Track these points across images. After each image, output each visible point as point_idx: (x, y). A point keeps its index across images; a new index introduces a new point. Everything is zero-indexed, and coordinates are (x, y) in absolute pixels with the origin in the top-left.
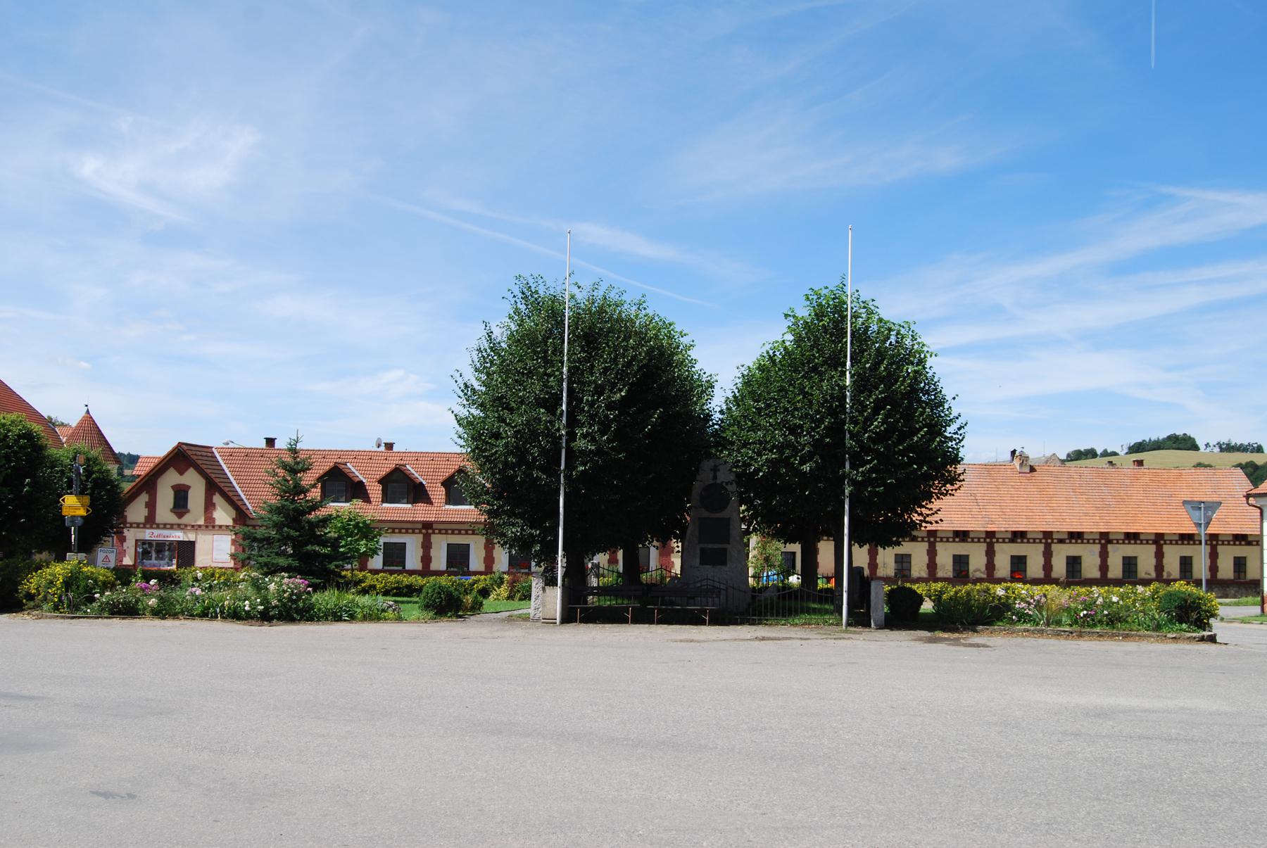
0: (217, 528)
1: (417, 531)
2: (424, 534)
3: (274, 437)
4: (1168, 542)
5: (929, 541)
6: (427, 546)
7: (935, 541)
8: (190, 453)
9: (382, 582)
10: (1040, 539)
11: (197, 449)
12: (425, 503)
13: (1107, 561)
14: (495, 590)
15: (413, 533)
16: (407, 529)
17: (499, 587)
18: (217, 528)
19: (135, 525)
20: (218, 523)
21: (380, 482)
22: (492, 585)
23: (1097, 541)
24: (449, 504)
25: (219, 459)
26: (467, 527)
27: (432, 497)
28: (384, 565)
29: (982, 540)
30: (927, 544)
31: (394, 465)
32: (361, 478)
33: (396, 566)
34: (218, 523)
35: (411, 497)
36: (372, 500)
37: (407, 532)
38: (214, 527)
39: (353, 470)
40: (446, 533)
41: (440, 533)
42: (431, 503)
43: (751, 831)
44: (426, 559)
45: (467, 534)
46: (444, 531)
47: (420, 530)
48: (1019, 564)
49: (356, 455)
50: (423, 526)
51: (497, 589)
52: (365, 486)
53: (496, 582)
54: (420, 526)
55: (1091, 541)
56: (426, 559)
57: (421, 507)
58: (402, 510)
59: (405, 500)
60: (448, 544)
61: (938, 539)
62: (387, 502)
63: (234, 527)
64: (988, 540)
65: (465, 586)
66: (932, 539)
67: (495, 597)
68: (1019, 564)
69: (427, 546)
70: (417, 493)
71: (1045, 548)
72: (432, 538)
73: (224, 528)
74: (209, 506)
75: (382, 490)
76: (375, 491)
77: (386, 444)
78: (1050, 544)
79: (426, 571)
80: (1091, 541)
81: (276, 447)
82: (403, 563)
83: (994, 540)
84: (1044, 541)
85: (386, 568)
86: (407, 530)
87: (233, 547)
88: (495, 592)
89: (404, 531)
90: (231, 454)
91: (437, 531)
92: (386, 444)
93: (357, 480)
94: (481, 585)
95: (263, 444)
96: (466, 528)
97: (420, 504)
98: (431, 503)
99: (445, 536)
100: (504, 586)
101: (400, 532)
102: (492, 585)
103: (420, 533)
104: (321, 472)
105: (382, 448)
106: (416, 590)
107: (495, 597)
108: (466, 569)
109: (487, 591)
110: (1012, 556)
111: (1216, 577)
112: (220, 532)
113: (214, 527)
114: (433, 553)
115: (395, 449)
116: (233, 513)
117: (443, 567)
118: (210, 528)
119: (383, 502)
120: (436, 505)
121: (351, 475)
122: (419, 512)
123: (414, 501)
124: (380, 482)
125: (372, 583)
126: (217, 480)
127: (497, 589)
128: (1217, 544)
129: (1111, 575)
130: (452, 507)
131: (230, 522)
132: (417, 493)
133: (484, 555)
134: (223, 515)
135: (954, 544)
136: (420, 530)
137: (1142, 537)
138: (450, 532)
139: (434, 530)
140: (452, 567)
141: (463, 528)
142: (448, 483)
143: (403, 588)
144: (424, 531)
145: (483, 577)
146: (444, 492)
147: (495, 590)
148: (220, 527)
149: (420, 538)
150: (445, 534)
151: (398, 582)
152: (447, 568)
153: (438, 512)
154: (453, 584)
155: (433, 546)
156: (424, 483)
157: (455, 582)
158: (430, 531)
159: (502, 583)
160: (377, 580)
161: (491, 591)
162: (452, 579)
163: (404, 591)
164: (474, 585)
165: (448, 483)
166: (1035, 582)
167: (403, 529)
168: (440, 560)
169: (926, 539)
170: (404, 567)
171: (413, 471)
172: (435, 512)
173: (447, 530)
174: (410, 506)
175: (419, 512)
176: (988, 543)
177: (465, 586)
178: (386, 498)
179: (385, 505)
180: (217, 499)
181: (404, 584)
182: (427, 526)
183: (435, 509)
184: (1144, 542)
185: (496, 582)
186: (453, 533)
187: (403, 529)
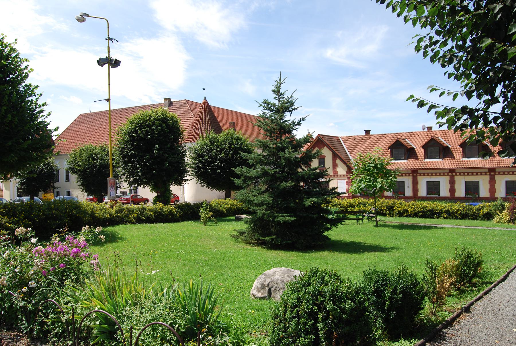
0: (339, 176)
1: (446, 174)
2: (450, 176)
3: (369, 129)
4: (458, 174)
5: (490, 175)
6: (452, 183)
7: (417, 176)
8: (324, 139)
9: (412, 207)
11: (329, 137)
12: (450, 158)
14: (498, 215)
15: (444, 175)
16: (440, 173)
17: (501, 212)
18: (339, 176)
19: (507, 173)
20: (339, 174)
21: (423, 147)
22: (495, 210)
23: (345, 176)
24: (465, 158)
25: (342, 142)
27: (454, 154)
30: (489, 176)
31: (431, 137)
32: (447, 145)
34: (339, 174)
35: (406, 156)
36: (419, 158)
37: (440, 175)
38: (337, 176)
39: (409, 142)
40: (464, 175)
41: (460, 175)
42: (454, 158)
44: (452, 190)
46: (463, 174)
47: (448, 173)
49: (410, 135)
51: (499, 214)
52: (415, 150)
53: (498, 208)
54: (447, 171)
57: (448, 160)
58: (437, 162)
59: (439, 157)
60: (465, 181)
62: (427, 158)
63: (347, 175)
65: (473, 211)
67: (498, 220)
69: (452, 183)
70: (410, 153)
71: (490, 178)
73: (342, 176)
74: (335, 166)
75: (463, 152)
76: (420, 152)
77: (427, 127)
79: (492, 198)
80: (483, 173)
81: (371, 134)
82: (438, 193)
87: (347, 186)
88: (497, 216)
89: (438, 174)
90: (347, 139)
91: (458, 174)
92: (428, 128)
93: (409, 147)
94: (486, 210)
95: (364, 133)
96: (439, 172)
97: (447, 159)
98: (454, 158)
100: (505, 212)
101: (436, 175)
102: (495, 210)
103: (448, 175)
104: (423, 143)
105: (426, 130)
106: (436, 213)
107: (498, 220)
108: (477, 196)
109: (492, 215)
112: (340, 178)
113: (337, 176)
115: (371, 133)
116: (346, 168)
118: (336, 176)
119: (425, 158)
120: (457, 158)
121: (406, 145)
122: (447, 163)
123: (444, 157)
124: (423, 147)
125: (405, 208)
126: (337, 152)
127: (499, 214)
128: (495, 174)
130: (467, 159)
131: (345, 173)
132: (410, 153)
133: (489, 187)
134: (341, 170)
136: (448, 173)
137: (419, 171)
138: (466, 174)
139: (456, 173)
140: (508, 195)
142: (425, 147)
143: (427, 212)
144: (450, 174)
145: (487, 204)
146: (462, 151)
147: (498, 215)
148: (340, 175)
149: (448, 178)
151: (423, 208)
152: (506, 196)
153: (499, 162)
154: (464, 209)
155: (456, 182)
156: (449, 146)
157: (466, 207)
158: (454, 174)
159: (503, 209)
160: (409, 206)
161: (495, 215)
162: (463, 205)
163: (428, 214)
164: (480, 210)
165: (425, 147)
168: (460, 191)
169: (411, 175)
171: (442, 140)
172: (456, 163)
173: (464, 173)
174: (441, 160)
175: (447, 163)
177: (473, 211)
178: (427, 156)
179: (426, 160)
180: (338, 161)
181: (428, 209)
182: (452, 172)
183: (457, 161)
185: (498, 208)
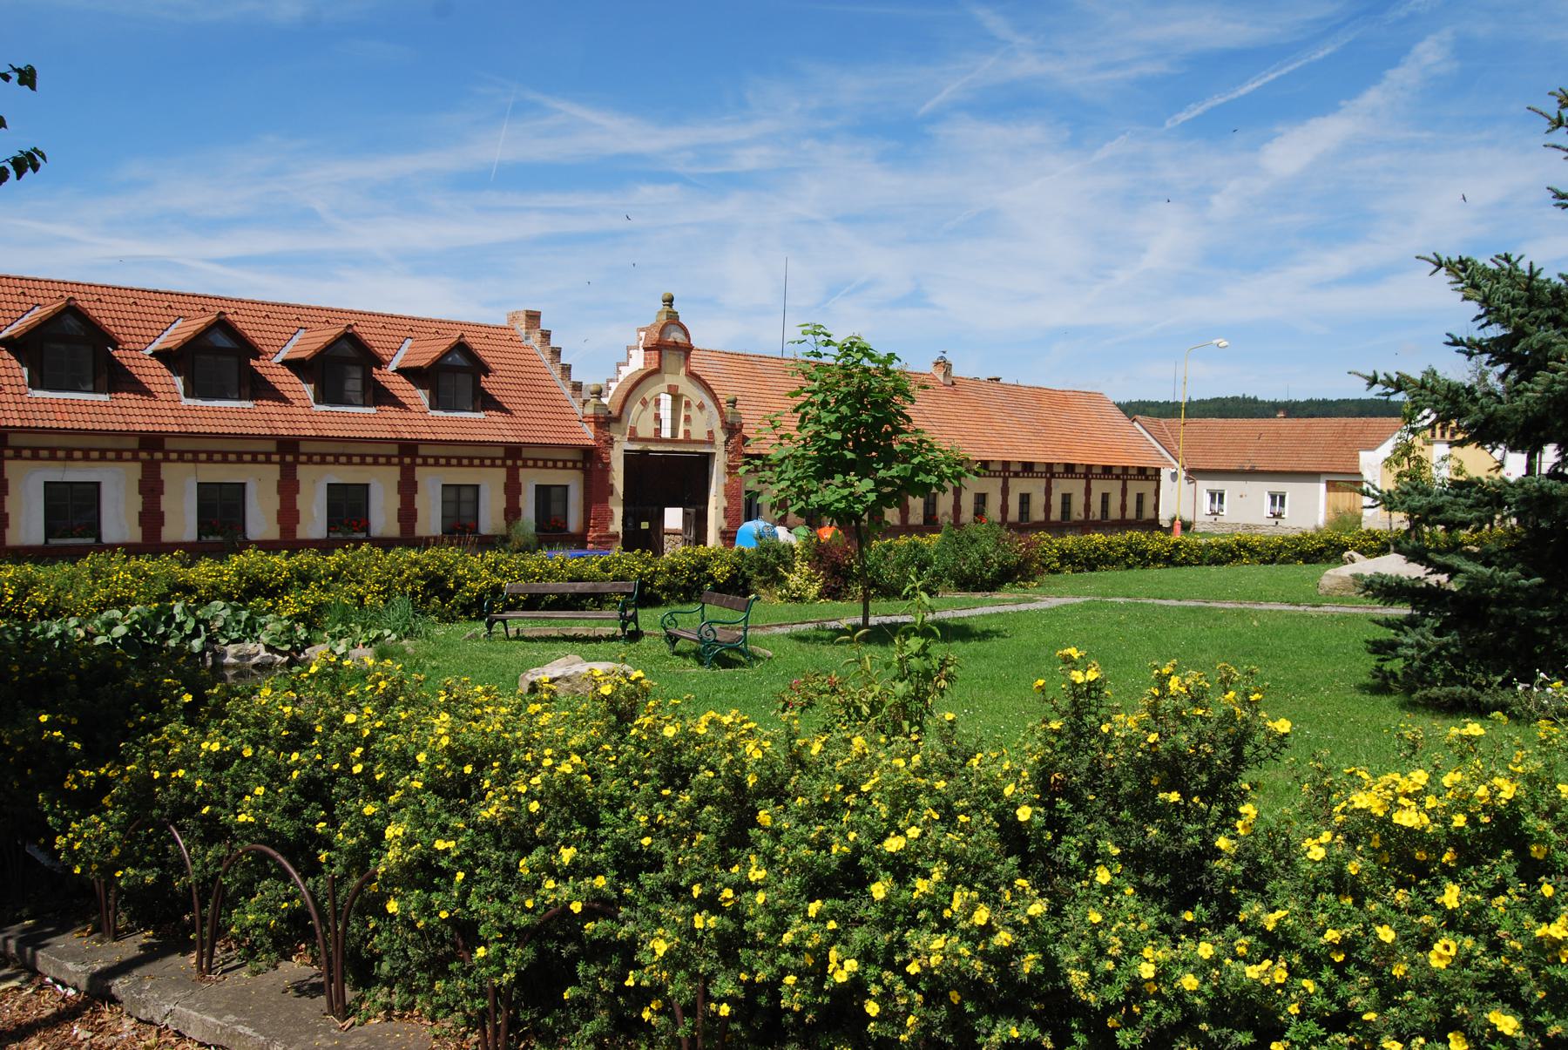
1: (127, 455)
4: (174, 456)
5: (282, 463)
6: (151, 489)
10: (575, 462)
13: (402, 502)
15: (119, 458)
23: (499, 462)
26: (106, 443)
28: (50, 532)
29: (499, 462)
30: (277, 467)
33: (81, 536)
37: (103, 458)
41: (181, 459)
43: (1278, 832)
44: (407, 515)
45: (363, 463)
46: (190, 456)
47: (135, 453)
48: (461, 507)
50: (141, 444)
55: (443, 461)
56: (407, 515)
59: (90, 387)
61: (419, 461)
62: (42, 387)
64: (509, 462)
66: (407, 460)
68: (461, 507)
72: (6, 469)
78: (157, 464)
83: (520, 463)
84: (276, 458)
85: (53, 542)
86: (376, 457)
89: (95, 455)
91: (174, 456)
99: (192, 465)
103: (135, 459)
110: (46, 483)
111: (413, 532)
114: (166, 503)
117: (190, 533)
129: (169, 534)
133: (277, 506)
135: (553, 471)
136: (135, 453)
139: (166, 453)
141: (203, 448)
144: (143, 455)
150: (334, 463)
155: (167, 488)
158: (159, 455)
166: (386, 544)
167: (330, 455)
169: (395, 460)
170: (368, 535)
173: (195, 453)
176: (508, 468)
184: (530, 463)
186: (210, 460)
187: (330, 455)
